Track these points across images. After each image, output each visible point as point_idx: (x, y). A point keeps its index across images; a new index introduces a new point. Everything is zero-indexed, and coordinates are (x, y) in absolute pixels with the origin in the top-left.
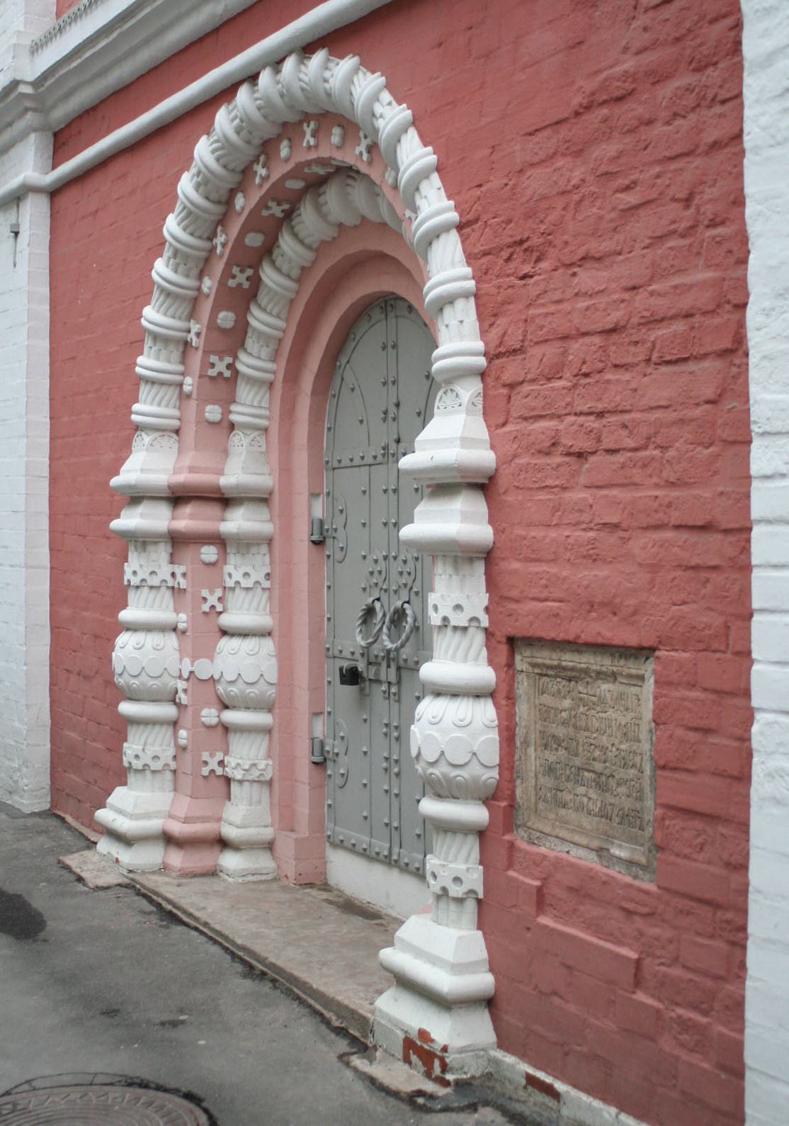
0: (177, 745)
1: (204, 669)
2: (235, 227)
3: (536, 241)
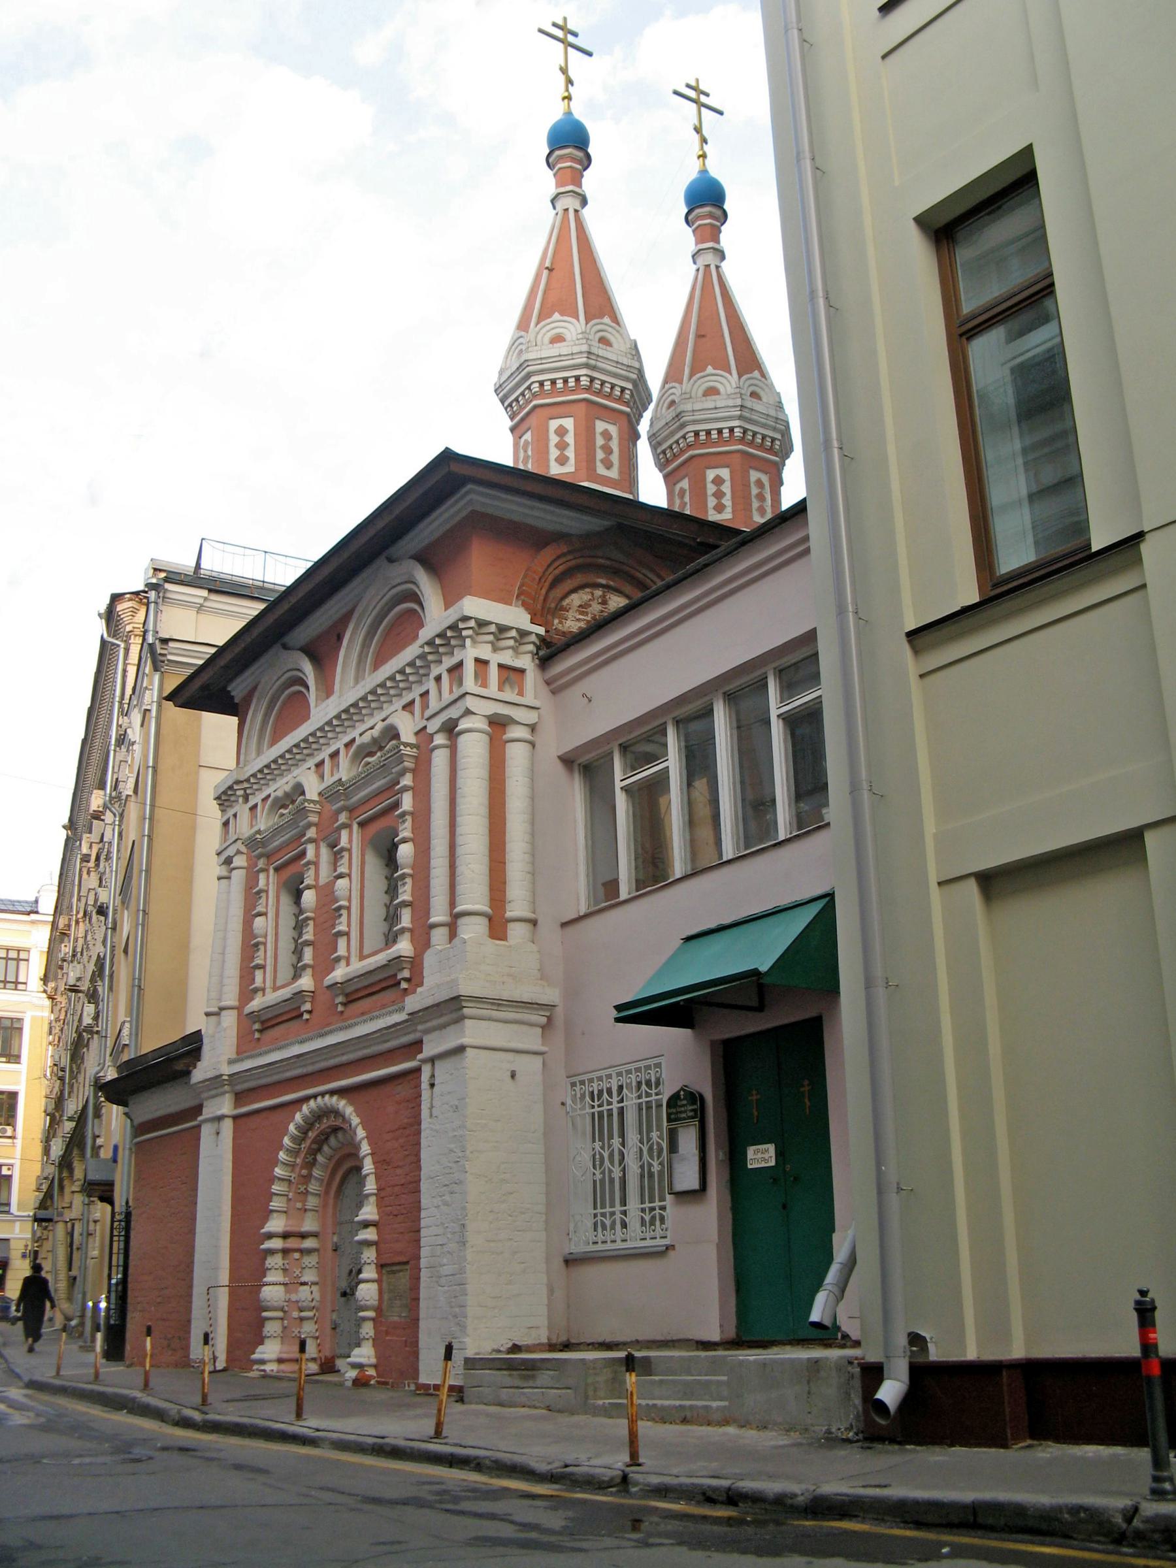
0: (283, 1325)
1: (294, 1297)
2: (308, 1142)
3: (388, 1160)
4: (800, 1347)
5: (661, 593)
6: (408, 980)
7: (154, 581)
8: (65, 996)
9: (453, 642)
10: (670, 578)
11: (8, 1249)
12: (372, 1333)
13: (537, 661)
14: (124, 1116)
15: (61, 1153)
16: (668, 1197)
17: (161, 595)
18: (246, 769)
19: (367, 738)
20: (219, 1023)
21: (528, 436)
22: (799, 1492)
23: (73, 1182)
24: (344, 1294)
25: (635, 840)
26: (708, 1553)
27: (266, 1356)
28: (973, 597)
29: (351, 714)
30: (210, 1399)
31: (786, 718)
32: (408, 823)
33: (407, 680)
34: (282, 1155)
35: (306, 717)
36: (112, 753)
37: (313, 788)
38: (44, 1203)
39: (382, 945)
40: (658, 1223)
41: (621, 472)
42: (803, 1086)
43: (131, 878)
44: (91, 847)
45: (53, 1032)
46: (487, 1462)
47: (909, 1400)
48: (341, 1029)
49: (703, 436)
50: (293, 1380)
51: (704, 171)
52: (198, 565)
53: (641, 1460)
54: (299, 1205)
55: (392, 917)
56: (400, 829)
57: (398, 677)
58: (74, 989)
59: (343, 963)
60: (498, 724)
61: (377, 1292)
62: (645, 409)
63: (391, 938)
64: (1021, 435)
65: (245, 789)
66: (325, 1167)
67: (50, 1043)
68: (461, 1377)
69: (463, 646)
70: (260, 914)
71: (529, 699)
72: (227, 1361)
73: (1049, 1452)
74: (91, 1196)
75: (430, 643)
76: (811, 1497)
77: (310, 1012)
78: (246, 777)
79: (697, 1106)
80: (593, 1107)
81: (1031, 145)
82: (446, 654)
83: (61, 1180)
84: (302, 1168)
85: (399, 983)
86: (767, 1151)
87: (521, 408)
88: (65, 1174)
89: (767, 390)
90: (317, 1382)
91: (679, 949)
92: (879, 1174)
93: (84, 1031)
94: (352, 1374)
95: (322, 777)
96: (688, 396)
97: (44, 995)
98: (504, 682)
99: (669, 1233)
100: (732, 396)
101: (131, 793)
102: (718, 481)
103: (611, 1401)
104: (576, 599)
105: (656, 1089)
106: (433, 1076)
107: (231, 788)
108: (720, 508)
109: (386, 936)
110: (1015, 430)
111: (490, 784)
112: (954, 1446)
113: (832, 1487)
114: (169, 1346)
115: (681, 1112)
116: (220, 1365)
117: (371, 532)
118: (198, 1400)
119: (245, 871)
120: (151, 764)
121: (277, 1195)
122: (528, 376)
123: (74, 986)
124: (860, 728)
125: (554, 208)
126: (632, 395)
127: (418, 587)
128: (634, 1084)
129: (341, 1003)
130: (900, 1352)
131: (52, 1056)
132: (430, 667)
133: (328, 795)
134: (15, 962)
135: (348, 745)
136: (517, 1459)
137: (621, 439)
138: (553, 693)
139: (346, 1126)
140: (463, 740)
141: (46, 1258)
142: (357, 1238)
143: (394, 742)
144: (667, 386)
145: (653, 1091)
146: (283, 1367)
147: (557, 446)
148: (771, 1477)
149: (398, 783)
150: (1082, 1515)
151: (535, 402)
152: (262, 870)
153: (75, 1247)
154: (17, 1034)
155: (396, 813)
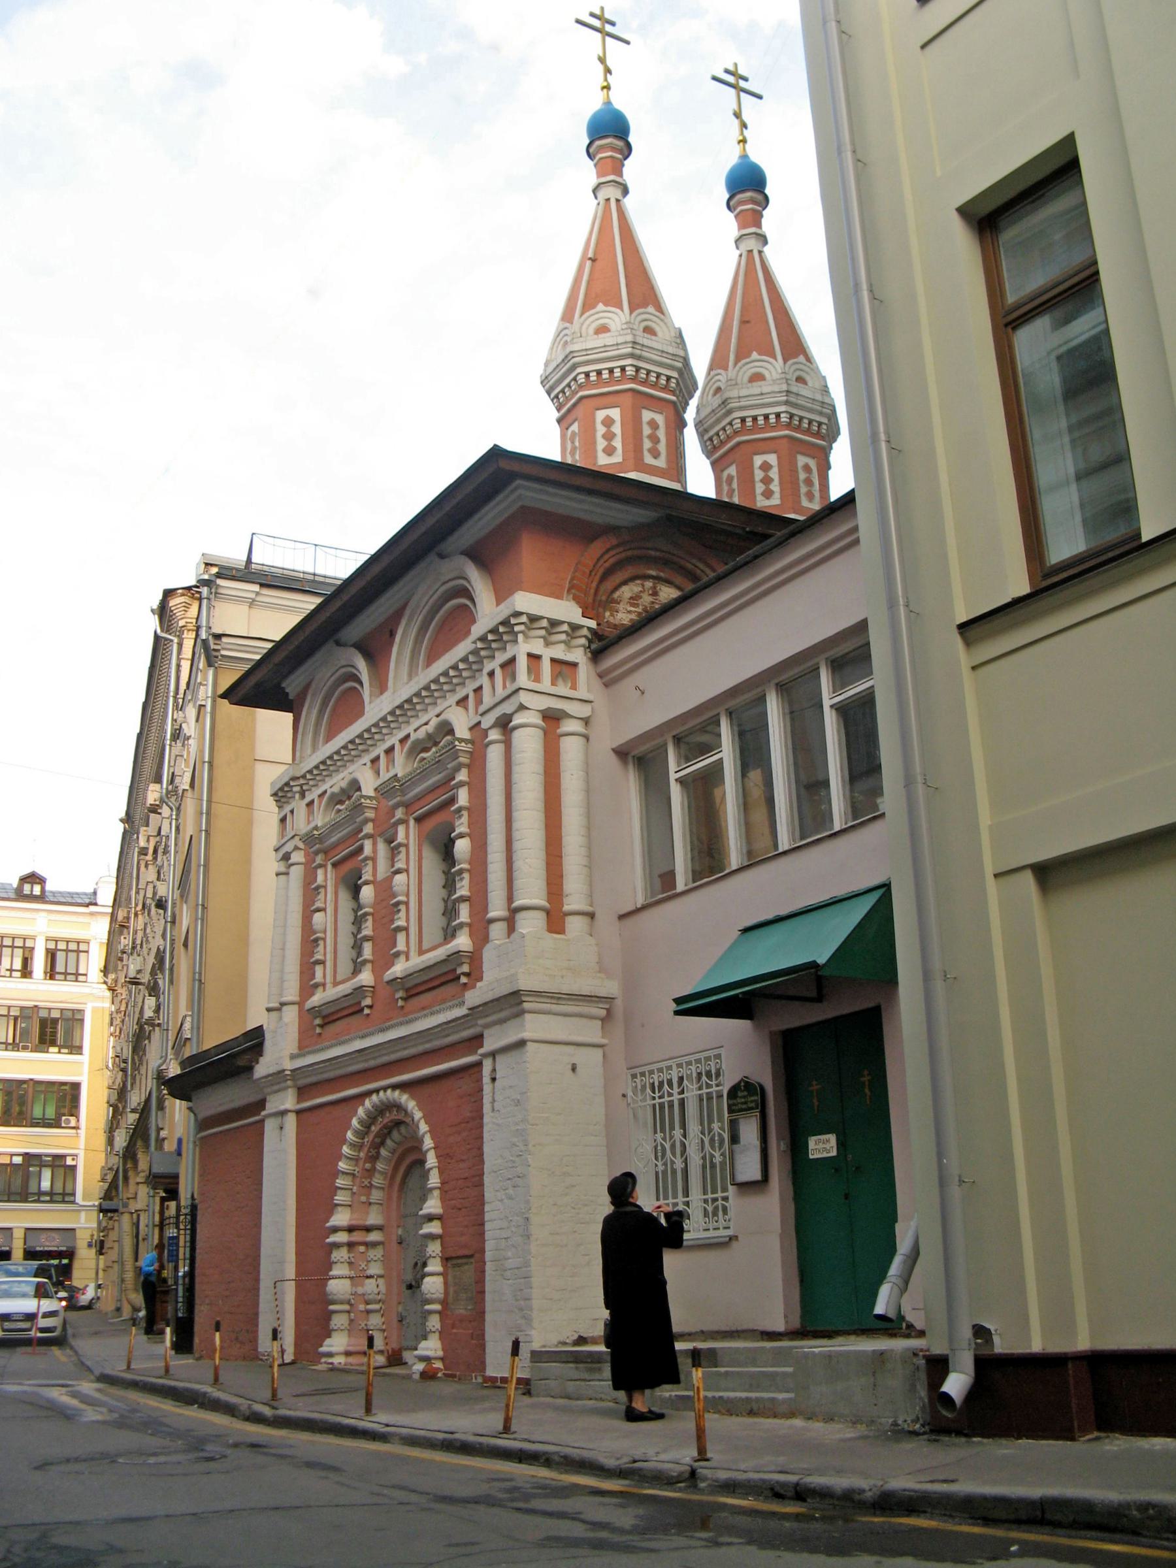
1: (360, 1290)
2: (371, 1136)
4: (865, 1336)
5: (713, 584)
6: (467, 975)
7: (206, 577)
8: (125, 988)
9: (505, 638)
10: (721, 569)
11: (75, 1238)
12: (438, 1326)
13: (589, 655)
14: (187, 1111)
15: (125, 1144)
16: (730, 1188)
17: (213, 590)
18: (302, 765)
19: (421, 734)
20: (281, 1018)
21: (575, 427)
22: (867, 1488)
23: (137, 1174)
24: (410, 1287)
25: (691, 831)
26: (778, 1553)
27: (333, 1349)
28: (1025, 589)
29: (405, 710)
30: (279, 1395)
31: (840, 709)
32: (465, 819)
33: (460, 676)
34: (345, 1149)
35: (361, 713)
36: (167, 748)
37: (369, 785)
38: (108, 1195)
39: (442, 940)
40: (720, 1213)
41: (668, 461)
42: (863, 1076)
43: (189, 872)
44: (148, 841)
45: (114, 1024)
46: (556, 1458)
47: (974, 1393)
48: (401, 1024)
49: (749, 423)
50: (362, 1373)
51: (744, 157)
52: (249, 561)
53: (709, 1455)
54: (363, 1199)
55: (450, 912)
56: (457, 824)
57: (452, 673)
58: (135, 982)
59: (402, 958)
60: (552, 718)
61: (442, 1285)
62: (691, 397)
63: (450, 933)
64: (1068, 415)
65: (301, 786)
66: (388, 1160)
67: (111, 1034)
68: (528, 1370)
69: (516, 641)
70: (318, 910)
71: (582, 693)
72: (295, 1354)
73: (1117, 1444)
74: (156, 1189)
75: (483, 639)
76: (878, 1493)
77: (370, 1007)
78: (302, 773)
79: (757, 1098)
80: (654, 1098)
81: (1072, 134)
82: (498, 649)
83: (125, 1172)
84: (365, 1162)
85: (458, 978)
86: (828, 1141)
87: (568, 399)
88: (129, 1165)
89: (812, 373)
90: (385, 1375)
91: (736, 941)
92: (941, 1167)
93: (146, 1024)
94: (420, 1367)
95: (378, 773)
96: (734, 382)
97: (105, 986)
98: (557, 676)
99: (731, 1224)
100: (778, 382)
101: (187, 787)
102: (766, 467)
103: (677, 1393)
104: (627, 591)
105: (716, 1080)
106: (494, 1070)
107: (287, 784)
108: (768, 494)
109: (445, 930)
110: (1061, 408)
111: (545, 777)
112: (1021, 1439)
113: (902, 1483)
114: (237, 1339)
115: (742, 1103)
116: (289, 1358)
117: (422, 528)
118: (268, 1394)
119: (302, 867)
120: (207, 759)
121: (342, 1189)
122: (574, 367)
123: (135, 978)
124: (910, 692)
125: (596, 198)
126: (678, 384)
127: (469, 582)
128: (694, 1075)
129: (401, 998)
130: (965, 1344)
131: (114, 1047)
132: (482, 662)
133: (383, 791)
134: (75, 954)
135: (403, 741)
136: (586, 1454)
137: (667, 427)
138: (606, 685)
139: (408, 1120)
140: (517, 735)
141: (112, 1248)
142: (421, 1232)
143: (449, 738)
144: (712, 373)
145: (714, 1083)
146: (351, 1360)
147: (604, 436)
148: (839, 1472)
149: (454, 778)
150: (1151, 1512)
151: (581, 394)
152: (320, 866)
153: (140, 1238)
154: (79, 1025)
155: (453, 808)
